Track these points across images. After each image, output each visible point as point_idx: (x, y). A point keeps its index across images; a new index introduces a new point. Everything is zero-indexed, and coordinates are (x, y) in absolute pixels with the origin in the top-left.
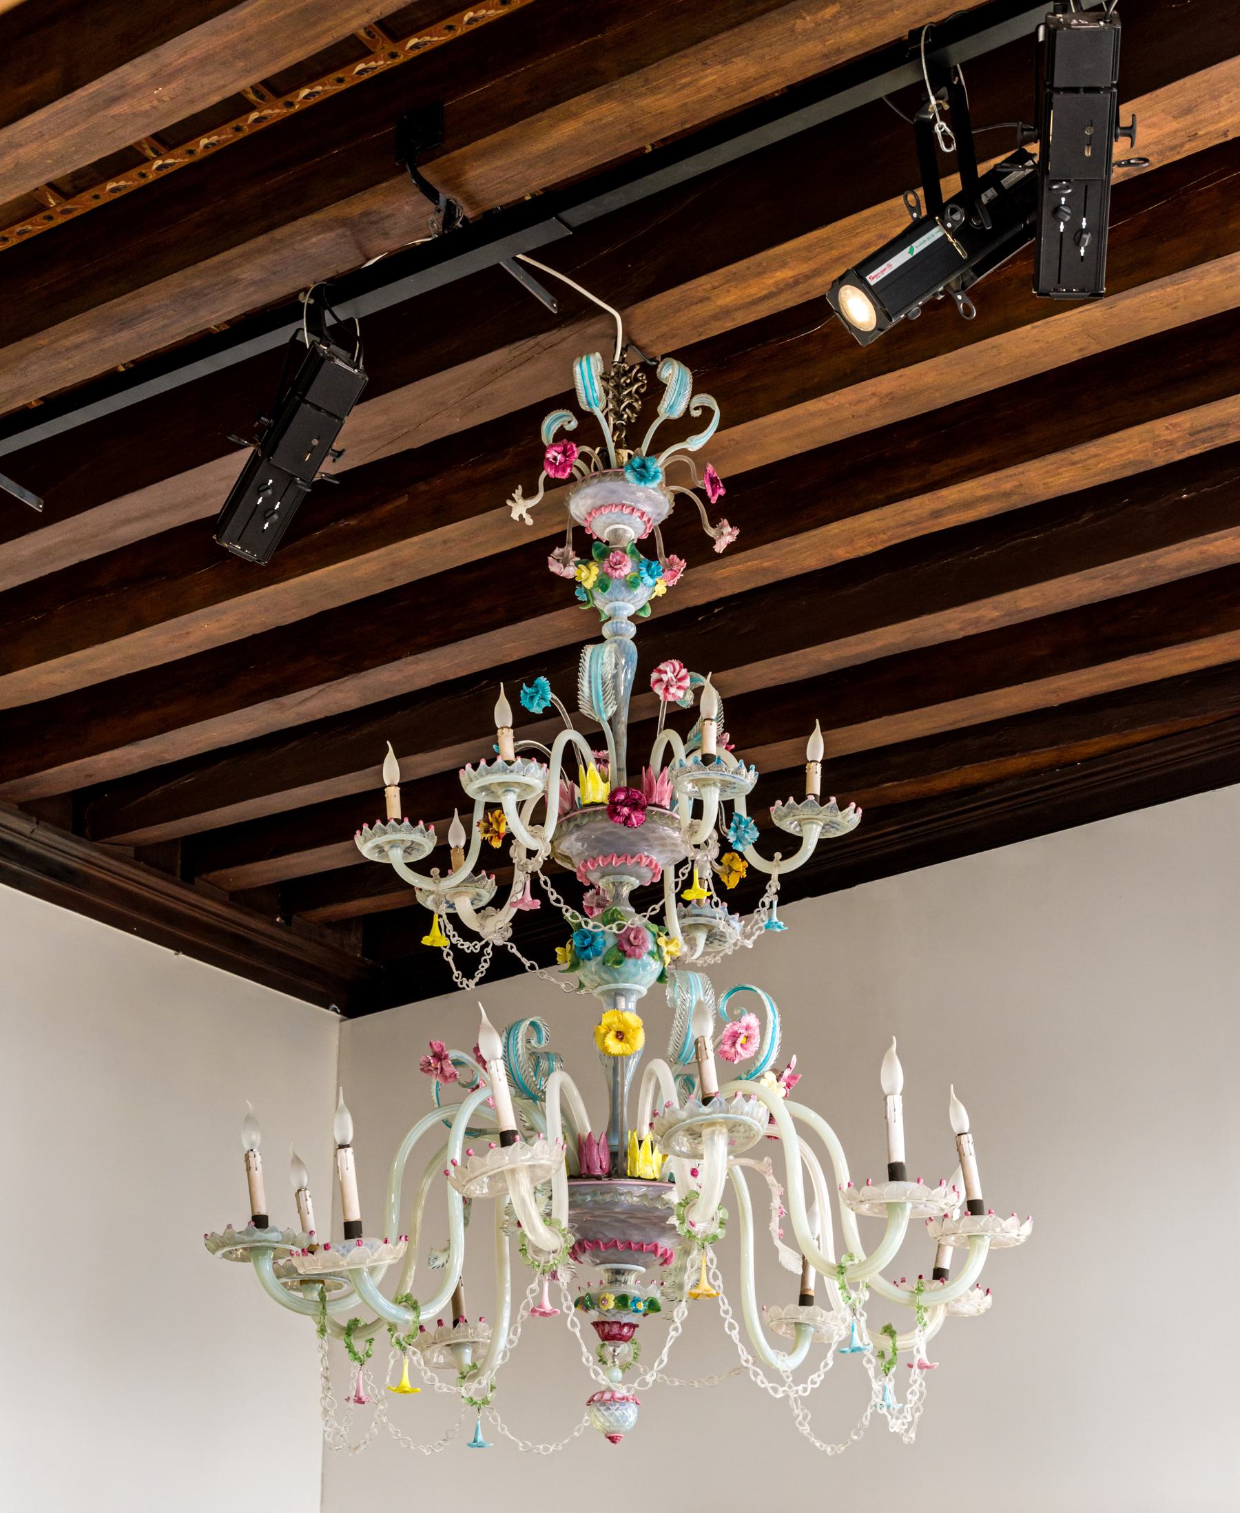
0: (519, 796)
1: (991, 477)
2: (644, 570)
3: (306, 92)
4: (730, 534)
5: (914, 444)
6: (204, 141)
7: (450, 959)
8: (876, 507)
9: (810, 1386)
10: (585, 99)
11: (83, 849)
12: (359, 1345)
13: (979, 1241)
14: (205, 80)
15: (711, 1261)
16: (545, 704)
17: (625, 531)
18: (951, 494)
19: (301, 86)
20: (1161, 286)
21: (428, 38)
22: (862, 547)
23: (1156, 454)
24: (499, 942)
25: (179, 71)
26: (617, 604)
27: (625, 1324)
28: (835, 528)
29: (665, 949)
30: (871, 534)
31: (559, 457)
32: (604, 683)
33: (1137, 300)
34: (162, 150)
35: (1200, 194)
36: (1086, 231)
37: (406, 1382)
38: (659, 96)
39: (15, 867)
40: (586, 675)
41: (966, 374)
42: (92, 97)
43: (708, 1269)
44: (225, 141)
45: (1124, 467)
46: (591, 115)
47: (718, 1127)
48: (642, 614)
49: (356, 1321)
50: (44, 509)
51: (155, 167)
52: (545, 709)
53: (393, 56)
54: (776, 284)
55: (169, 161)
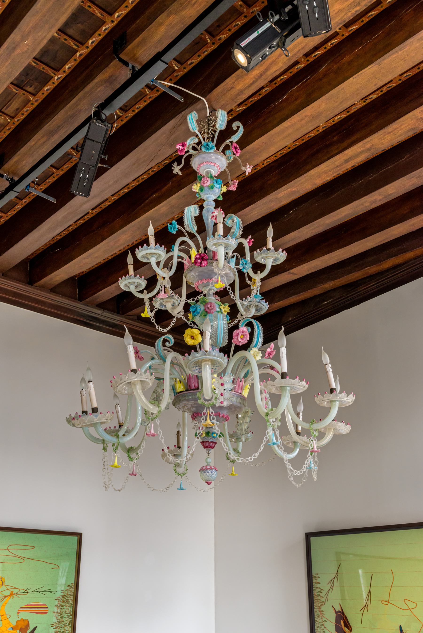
0: (157, 259)
1: (361, 144)
2: (215, 182)
3: (90, 42)
4: (250, 168)
5: (335, 138)
6: (67, 67)
7: (154, 321)
8: (324, 162)
9: (253, 458)
10: (163, 16)
11: (120, 318)
12: (133, 455)
13: (334, 403)
14: (39, 34)
15: (212, 413)
16: (176, 230)
17: (210, 171)
18: (349, 152)
19: (88, 39)
20: (396, 52)
21: (121, 12)
22: (325, 178)
23: (419, 124)
24: (179, 316)
25: (29, 32)
26: (207, 195)
27: (211, 442)
28: (312, 172)
29: (223, 310)
30: (325, 172)
31: (181, 147)
32: (191, 218)
33: (389, 60)
34: (56, 72)
35: (407, 14)
36: (316, 7)
37: (116, 463)
38: (187, 10)
39: (98, 324)
40: (186, 217)
41: (336, 102)
42: (7, 48)
43: (210, 416)
44: (73, 65)
45: (409, 131)
46: (167, 22)
47: (207, 362)
48: (219, 199)
49: (132, 448)
50: (56, 202)
51: (56, 79)
52: (177, 232)
53: (113, 22)
54: (254, 77)
55: (59, 76)
